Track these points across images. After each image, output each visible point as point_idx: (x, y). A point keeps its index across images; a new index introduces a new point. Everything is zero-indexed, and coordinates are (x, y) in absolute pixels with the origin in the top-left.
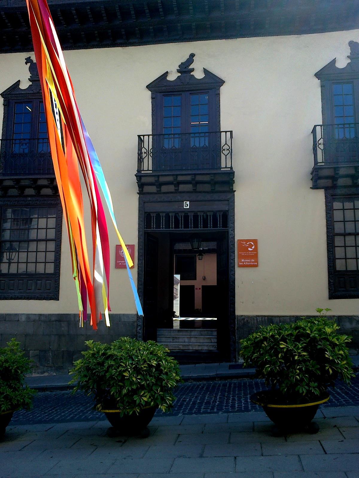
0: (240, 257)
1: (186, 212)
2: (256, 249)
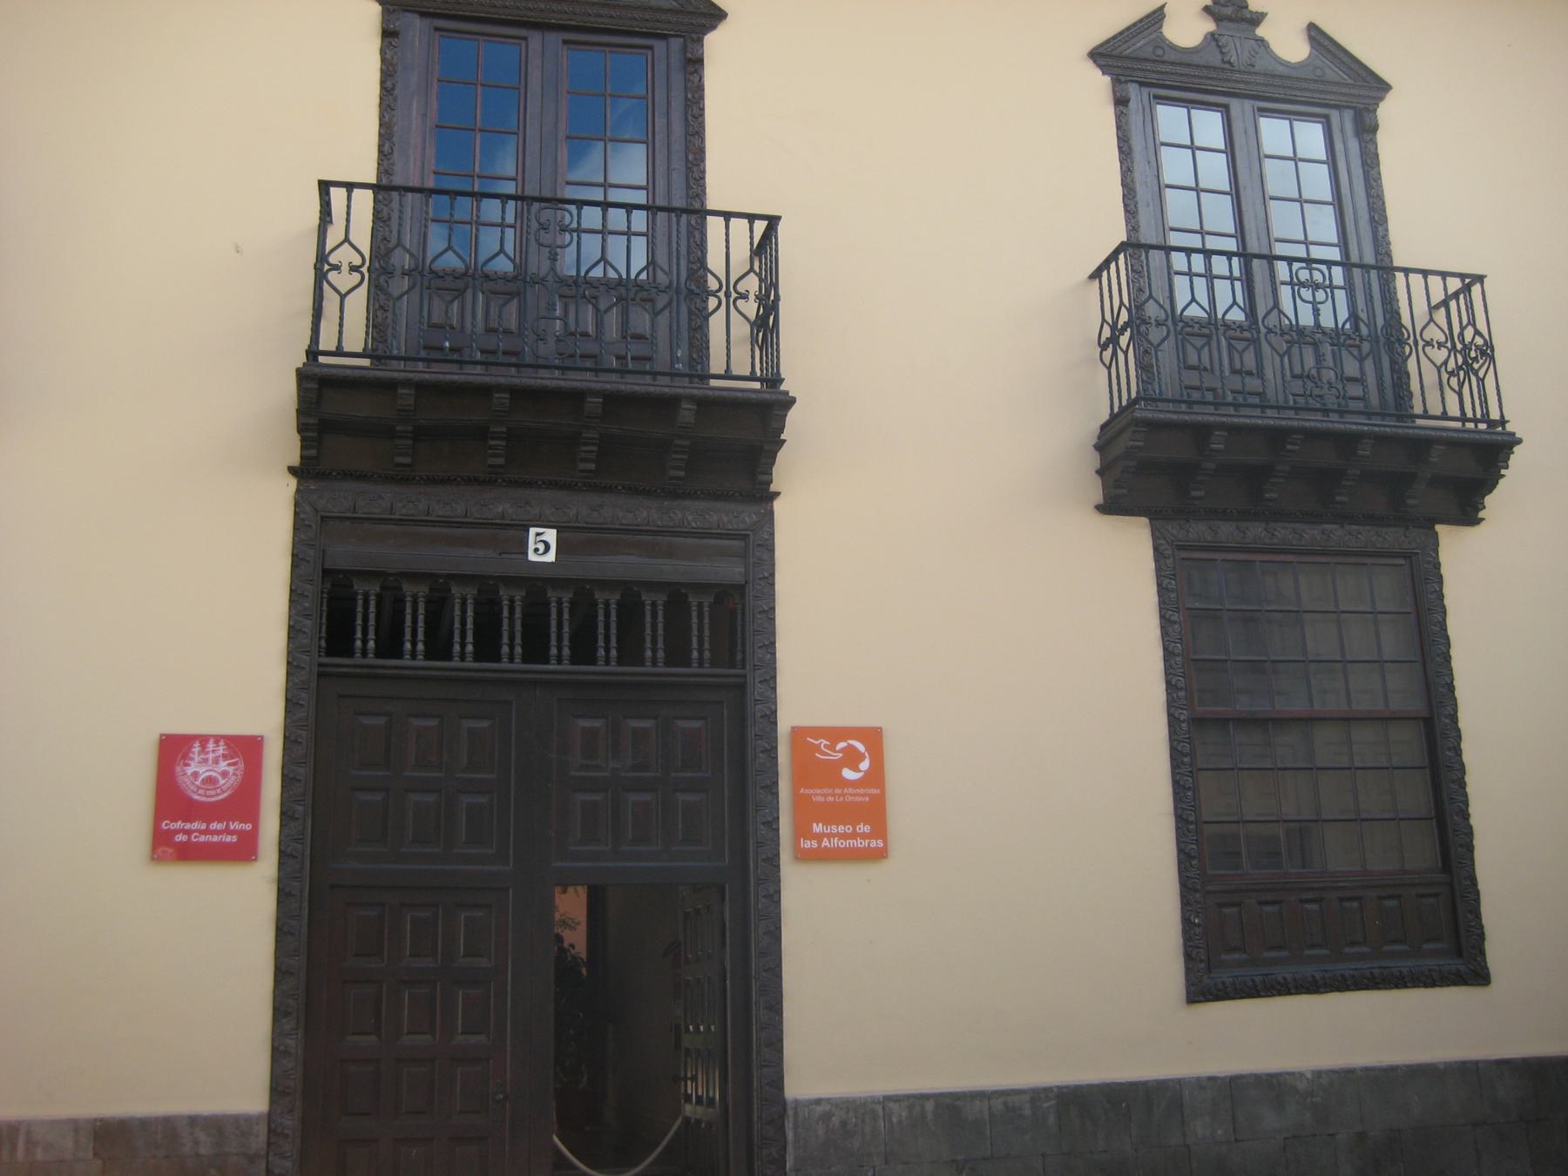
0: (806, 813)
1: (538, 583)
2: (876, 776)
